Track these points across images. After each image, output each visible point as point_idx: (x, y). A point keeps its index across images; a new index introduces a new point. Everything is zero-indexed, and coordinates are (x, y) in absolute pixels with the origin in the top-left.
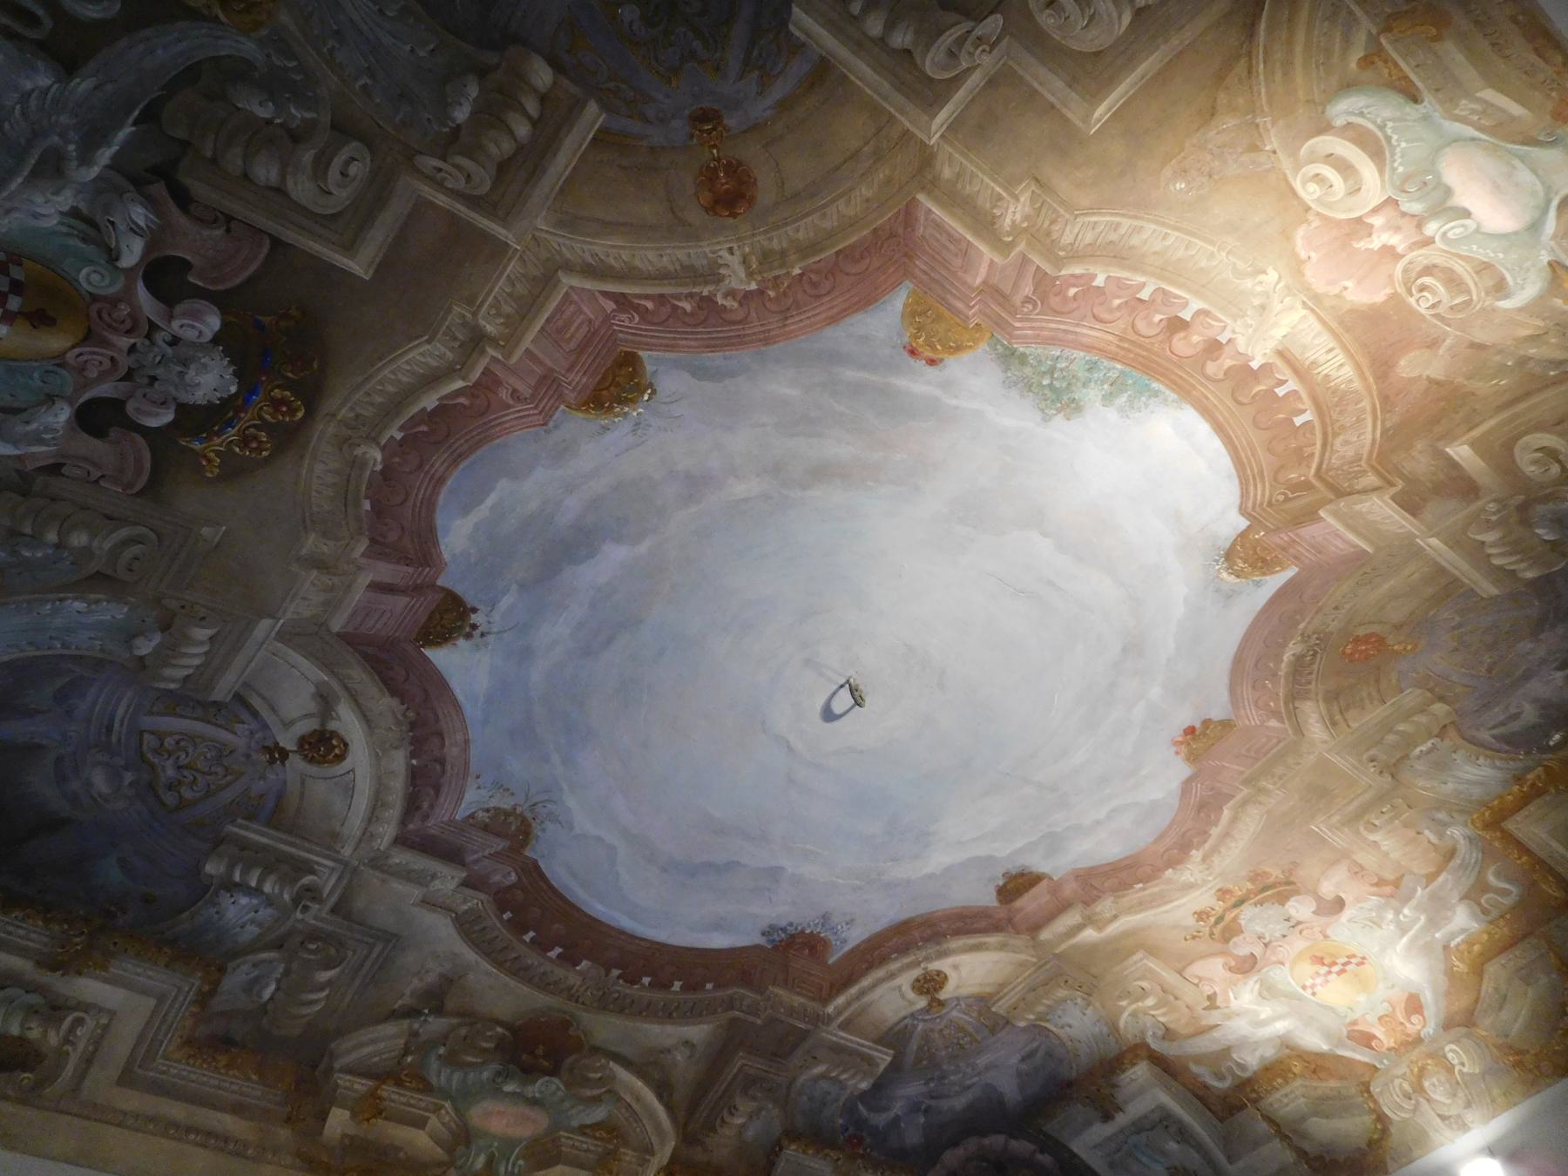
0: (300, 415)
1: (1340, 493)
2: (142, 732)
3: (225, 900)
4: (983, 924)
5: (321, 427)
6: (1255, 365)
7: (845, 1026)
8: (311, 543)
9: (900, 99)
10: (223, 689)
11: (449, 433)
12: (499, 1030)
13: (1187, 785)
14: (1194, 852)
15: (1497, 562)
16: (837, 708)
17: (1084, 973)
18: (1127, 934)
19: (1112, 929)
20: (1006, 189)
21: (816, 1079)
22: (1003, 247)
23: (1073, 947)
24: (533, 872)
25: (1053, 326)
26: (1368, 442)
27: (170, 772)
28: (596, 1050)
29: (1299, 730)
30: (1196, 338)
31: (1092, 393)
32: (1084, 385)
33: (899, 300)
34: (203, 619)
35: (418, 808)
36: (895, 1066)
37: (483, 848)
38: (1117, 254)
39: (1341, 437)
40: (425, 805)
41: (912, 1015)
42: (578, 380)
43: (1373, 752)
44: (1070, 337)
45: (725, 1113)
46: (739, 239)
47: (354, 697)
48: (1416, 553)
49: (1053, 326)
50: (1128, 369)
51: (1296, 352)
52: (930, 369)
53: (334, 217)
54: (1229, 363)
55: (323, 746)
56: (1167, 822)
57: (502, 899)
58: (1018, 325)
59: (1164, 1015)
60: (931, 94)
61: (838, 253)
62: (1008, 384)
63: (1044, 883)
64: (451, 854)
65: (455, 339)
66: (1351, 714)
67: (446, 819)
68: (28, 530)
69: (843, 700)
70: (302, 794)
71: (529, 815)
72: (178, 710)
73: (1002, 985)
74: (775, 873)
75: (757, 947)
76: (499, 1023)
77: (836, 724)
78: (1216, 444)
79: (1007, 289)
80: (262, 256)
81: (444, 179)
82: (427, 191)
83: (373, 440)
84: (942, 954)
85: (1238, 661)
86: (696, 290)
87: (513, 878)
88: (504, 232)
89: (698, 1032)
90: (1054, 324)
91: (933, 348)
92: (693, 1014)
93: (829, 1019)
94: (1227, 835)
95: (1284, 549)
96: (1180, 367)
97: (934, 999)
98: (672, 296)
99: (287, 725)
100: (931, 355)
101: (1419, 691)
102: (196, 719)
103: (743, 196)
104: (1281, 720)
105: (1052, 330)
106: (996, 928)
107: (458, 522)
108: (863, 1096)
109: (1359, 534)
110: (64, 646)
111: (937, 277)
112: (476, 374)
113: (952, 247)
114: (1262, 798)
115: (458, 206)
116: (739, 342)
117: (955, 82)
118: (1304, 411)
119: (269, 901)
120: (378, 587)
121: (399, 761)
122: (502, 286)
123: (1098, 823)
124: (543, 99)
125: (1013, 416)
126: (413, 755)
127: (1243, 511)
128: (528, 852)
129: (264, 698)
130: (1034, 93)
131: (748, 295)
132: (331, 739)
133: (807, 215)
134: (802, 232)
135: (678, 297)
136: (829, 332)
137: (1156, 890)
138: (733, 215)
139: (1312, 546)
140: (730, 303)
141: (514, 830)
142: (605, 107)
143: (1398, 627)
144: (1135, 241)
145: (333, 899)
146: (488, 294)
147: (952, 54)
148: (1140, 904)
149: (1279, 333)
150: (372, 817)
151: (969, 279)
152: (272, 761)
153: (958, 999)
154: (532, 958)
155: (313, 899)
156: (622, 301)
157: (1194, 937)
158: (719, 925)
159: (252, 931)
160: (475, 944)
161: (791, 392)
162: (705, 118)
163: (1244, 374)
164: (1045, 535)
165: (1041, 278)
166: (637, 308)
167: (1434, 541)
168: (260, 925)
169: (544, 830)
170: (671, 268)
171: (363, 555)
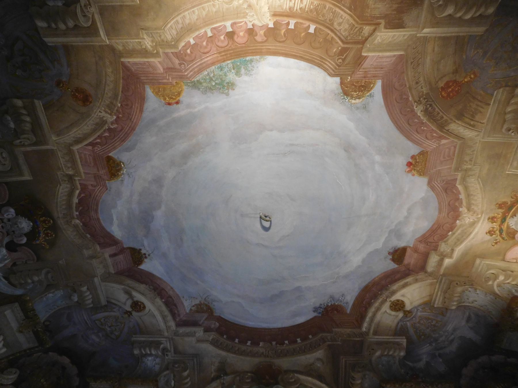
0: (51, 221)
1: (363, 42)
3: (145, 360)
4: (398, 276)
5: (59, 222)
6: (271, 25)
7: (376, 333)
8: (87, 253)
9: (88, 39)
10: (103, 302)
11: (87, 206)
12: (249, 374)
13: (430, 183)
14: (461, 209)
15: (468, 17)
17: (461, 275)
18: (465, 254)
20: (138, 39)
21: (380, 357)
22: (157, 55)
24: (220, 319)
25: (195, 66)
26: (348, 17)
27: (109, 329)
28: (287, 372)
29: (458, 137)
30: (241, 34)
33: (149, 92)
35: (175, 313)
36: (410, 342)
37: (202, 318)
38: (189, 29)
39: (335, 24)
40: (176, 312)
41: (401, 320)
43: (505, 126)
44: (204, 65)
45: (351, 380)
46: (99, 107)
47: (133, 288)
48: (425, 40)
50: (233, 61)
51: (278, 10)
52: (179, 105)
53: (11, 169)
54: (262, 32)
55: (138, 306)
57: (219, 331)
59: (513, 280)
60: (92, 30)
62: (205, 92)
63: (409, 251)
64: (195, 324)
65: (65, 181)
66: (478, 117)
68: (23, 282)
69: (267, 224)
70: (143, 322)
71: (206, 303)
73: (431, 296)
74: (298, 289)
75: (315, 317)
76: (247, 372)
77: (271, 230)
78: (292, 61)
80: (6, 189)
81: (24, 143)
82: (23, 149)
84: (394, 293)
85: (399, 128)
86: (104, 128)
87: (217, 324)
89: (320, 354)
91: (172, 98)
92: (312, 348)
93: (367, 333)
94: (469, 196)
96: (248, 47)
97: (405, 312)
100: (175, 101)
101: (501, 90)
104: (445, 138)
107: (113, 228)
108: (405, 358)
109: (390, 51)
110: (58, 307)
111: (151, 78)
112: (79, 186)
113: (145, 67)
114: (470, 173)
115: (33, 148)
116: (127, 136)
117: (94, 22)
118: (309, 26)
119: (157, 356)
120: (112, 256)
121: (159, 301)
123: (406, 218)
124: (24, 108)
125: (216, 102)
130: (113, 7)
131: (116, 120)
132: (138, 303)
133: (105, 89)
135: (102, 134)
137: (459, 231)
138: (91, 102)
139: (375, 68)
141: (205, 309)
143: (456, 72)
144: (187, 21)
145: (172, 349)
147: (85, 16)
148: (458, 240)
149: (266, 9)
150: (165, 322)
151: (159, 72)
152: (129, 316)
153: (415, 307)
154: (243, 348)
155: (167, 351)
157: (496, 243)
158: (295, 315)
159: (157, 368)
160: (222, 349)
161: (154, 139)
162: (58, 83)
163: (272, 33)
164: (271, 130)
165: (176, 55)
166: (97, 143)
167: (426, 30)
168: (159, 364)
169: (214, 305)
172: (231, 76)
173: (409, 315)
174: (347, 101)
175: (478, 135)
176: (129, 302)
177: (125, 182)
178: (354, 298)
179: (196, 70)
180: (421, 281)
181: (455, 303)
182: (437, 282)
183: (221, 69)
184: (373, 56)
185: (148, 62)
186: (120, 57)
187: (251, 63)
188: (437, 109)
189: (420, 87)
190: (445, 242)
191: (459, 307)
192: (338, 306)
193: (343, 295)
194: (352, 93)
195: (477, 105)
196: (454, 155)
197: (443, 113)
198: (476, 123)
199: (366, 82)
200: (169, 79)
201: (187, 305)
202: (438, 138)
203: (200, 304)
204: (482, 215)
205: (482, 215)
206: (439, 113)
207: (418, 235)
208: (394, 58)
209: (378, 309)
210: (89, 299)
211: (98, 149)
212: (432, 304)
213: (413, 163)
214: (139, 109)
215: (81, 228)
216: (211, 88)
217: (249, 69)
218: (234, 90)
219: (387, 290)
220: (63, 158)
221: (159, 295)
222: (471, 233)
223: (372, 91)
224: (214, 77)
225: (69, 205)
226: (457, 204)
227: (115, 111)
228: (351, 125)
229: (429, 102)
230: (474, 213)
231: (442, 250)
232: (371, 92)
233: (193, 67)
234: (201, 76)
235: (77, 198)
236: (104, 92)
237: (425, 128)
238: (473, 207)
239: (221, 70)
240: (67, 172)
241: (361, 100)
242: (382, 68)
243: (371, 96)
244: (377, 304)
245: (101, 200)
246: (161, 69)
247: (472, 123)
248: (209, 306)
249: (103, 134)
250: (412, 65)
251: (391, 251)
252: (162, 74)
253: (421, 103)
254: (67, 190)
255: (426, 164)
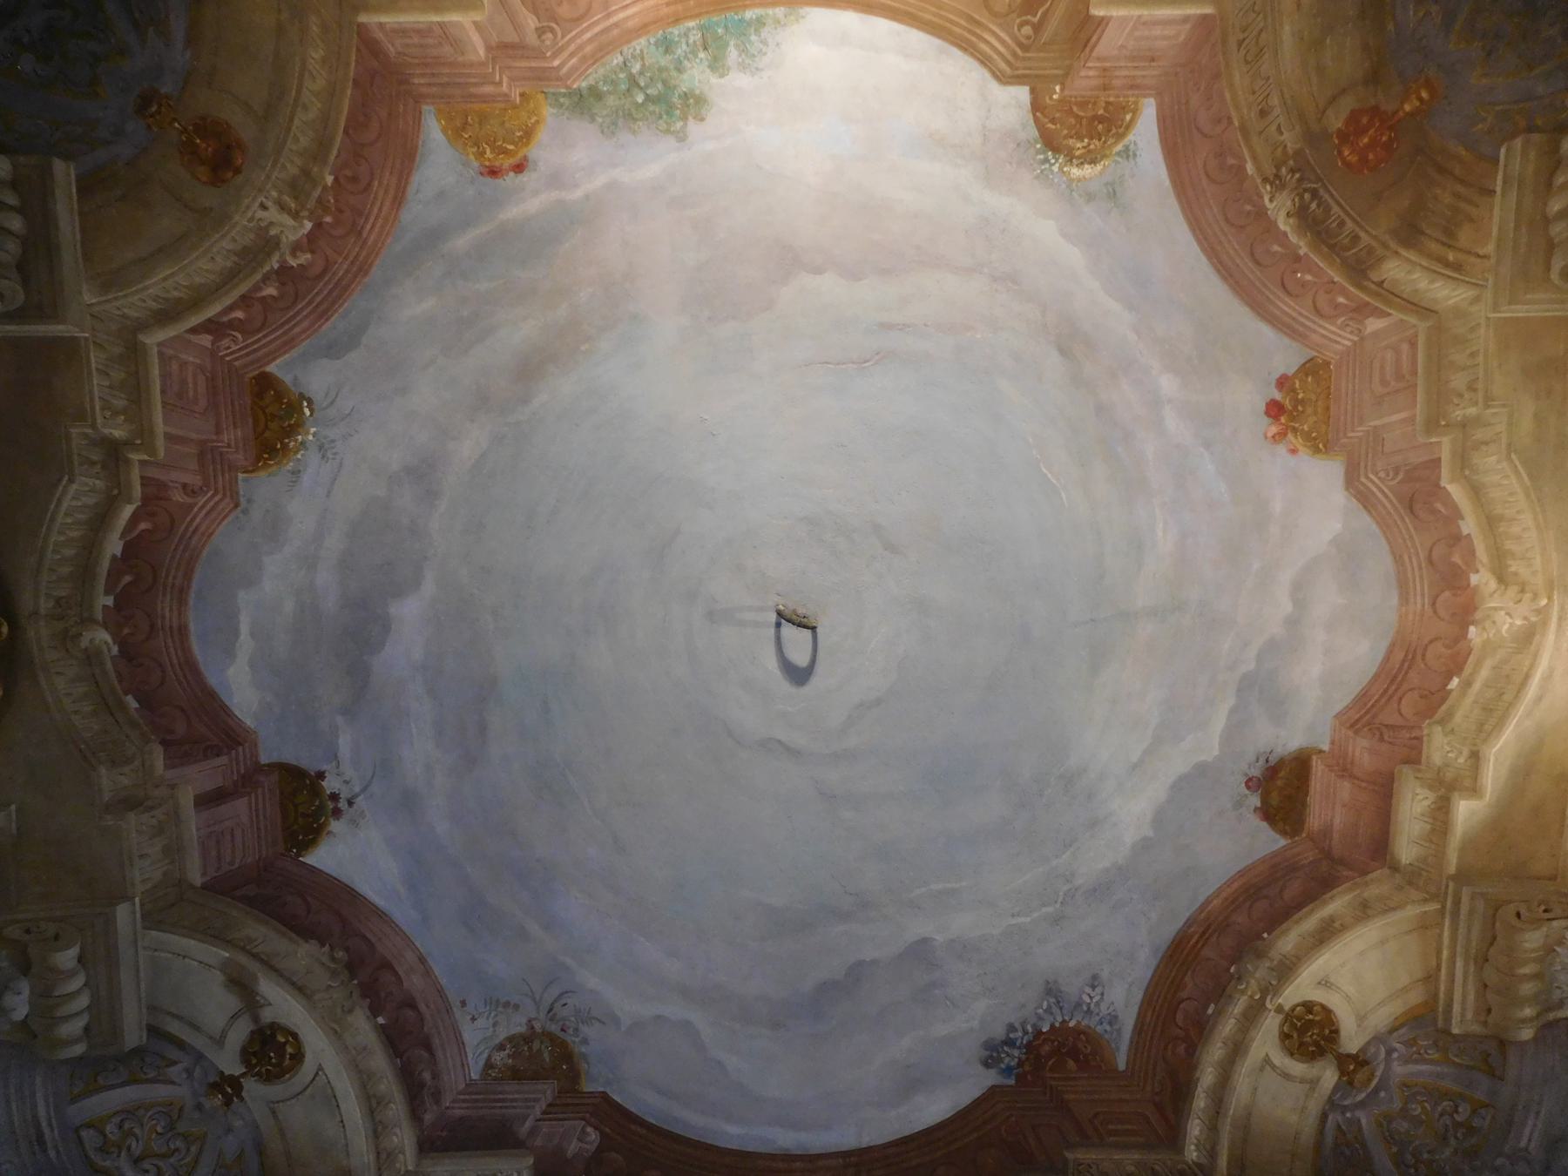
2: (77, 1130)
4: (1293, 889)
5: (32, 633)
8: (110, 781)
10: (133, 1036)
11: (153, 572)
13: (1352, 480)
14: (1474, 579)
16: (800, 658)
19: (1493, 776)
23: (1463, 849)
25: (588, 35)
31: (695, 72)
32: (680, 70)
33: (433, 130)
34: (57, 937)
35: (422, 1085)
40: (427, 1076)
41: (1332, 1104)
42: (233, 437)
44: (615, 32)
49: (588, 35)
52: (524, 178)
55: (271, 1051)
56: (1389, 559)
58: (556, 63)
61: (346, 132)
62: (609, 131)
63: (1318, 767)
65: (93, 463)
66: (1465, 236)
67: (462, 1086)
69: (797, 644)
70: (282, 1132)
71: (554, 1028)
72: (101, 1081)
73: (1430, 978)
74: (920, 951)
75: (992, 1093)
77: (817, 682)
79: (511, 37)
83: (87, 621)
84: (1287, 970)
85: (1227, 272)
86: (267, 268)
87: (593, 1135)
88: (61, 327)
90: (588, 33)
91: (506, 152)
94: (1491, 522)
95: (1105, 88)
97: (1343, 1060)
98: (249, 291)
99: (220, 1041)
100: (508, 162)
101: (1518, 143)
102: (123, 1084)
103: (229, 147)
105: (590, 40)
106: (1321, 884)
107: (231, 672)
111: (446, 79)
112: (137, 491)
113: (430, 41)
114: (1479, 434)
116: (341, 291)
120: (207, 801)
121: (363, 1028)
122: (98, 383)
123: (1293, 622)
125: (646, 161)
126: (374, 1011)
127: (1003, 79)
128: (587, 1087)
129: (179, 1018)
131: (311, 237)
132: (273, 1036)
133: (291, 120)
134: (303, 140)
135: (257, 288)
136: (406, 216)
137: (1484, 673)
138: (237, 171)
140: (304, 258)
142: (67, 157)
143: (1374, 78)
146: (92, 400)
148: (1488, 710)
150: (377, 1130)
151: (473, 58)
152: (228, 1103)
153: (1377, 1039)
156: (214, 327)
158: (912, 1082)
161: (429, 304)
162: (146, 101)
164: (818, 271)
166: (231, 325)
169: (585, 1041)
170: (229, 264)
171: (166, 767)
172: (697, 75)
173: (1360, 1077)
174: (1056, 168)
175: (1477, 300)
176: (240, 1032)
177: (306, 479)
178: (1138, 995)
179: (588, 49)
180: (1385, 912)
181: (1528, 1012)
182: (1442, 912)
183: (667, 46)
184: (1125, 19)
185: (441, 25)
186: (356, 9)
187: (757, 31)
188: (1335, 209)
189: (1273, 128)
190: (1442, 722)
191: (1548, 1029)
192: (1078, 1032)
193: (1094, 982)
194: (1071, 142)
195: (1457, 196)
196: (1415, 373)
197: (1354, 220)
198: (1461, 256)
199: (1108, 103)
200: (500, 83)
201: (477, 1040)
202: (1354, 310)
203: (528, 1038)
204: (1550, 598)
205: (1550, 598)
206: (1342, 224)
207: (1342, 699)
208: (1188, 26)
209: (1237, 1049)
210: (78, 992)
211: (231, 345)
212: (1440, 1024)
213: (1288, 404)
214: (391, 195)
215: (109, 666)
216: (630, 115)
217: (753, 51)
218: (702, 120)
219: (1260, 955)
220: (104, 373)
221: (364, 996)
222: (1527, 677)
223: (1130, 137)
224: (641, 73)
225: (84, 573)
226: (1457, 559)
227: (311, 204)
228: (1073, 256)
229: (1302, 173)
230: (1523, 591)
231: (1437, 759)
232: (1125, 141)
233: (579, 41)
234: (601, 71)
235: (123, 536)
236: (289, 129)
237: (1308, 277)
238: (1514, 566)
239: (667, 51)
240: (106, 431)
241: (1099, 167)
242: (1153, 60)
243: (1127, 153)
244: (1227, 1027)
245: (205, 553)
246: (478, 48)
247: (1451, 258)
248: (563, 1045)
249: (260, 289)
250: (1243, 52)
251: (1256, 772)
252: (482, 64)
253: (1283, 186)
254: (90, 500)
255: (1328, 408)
